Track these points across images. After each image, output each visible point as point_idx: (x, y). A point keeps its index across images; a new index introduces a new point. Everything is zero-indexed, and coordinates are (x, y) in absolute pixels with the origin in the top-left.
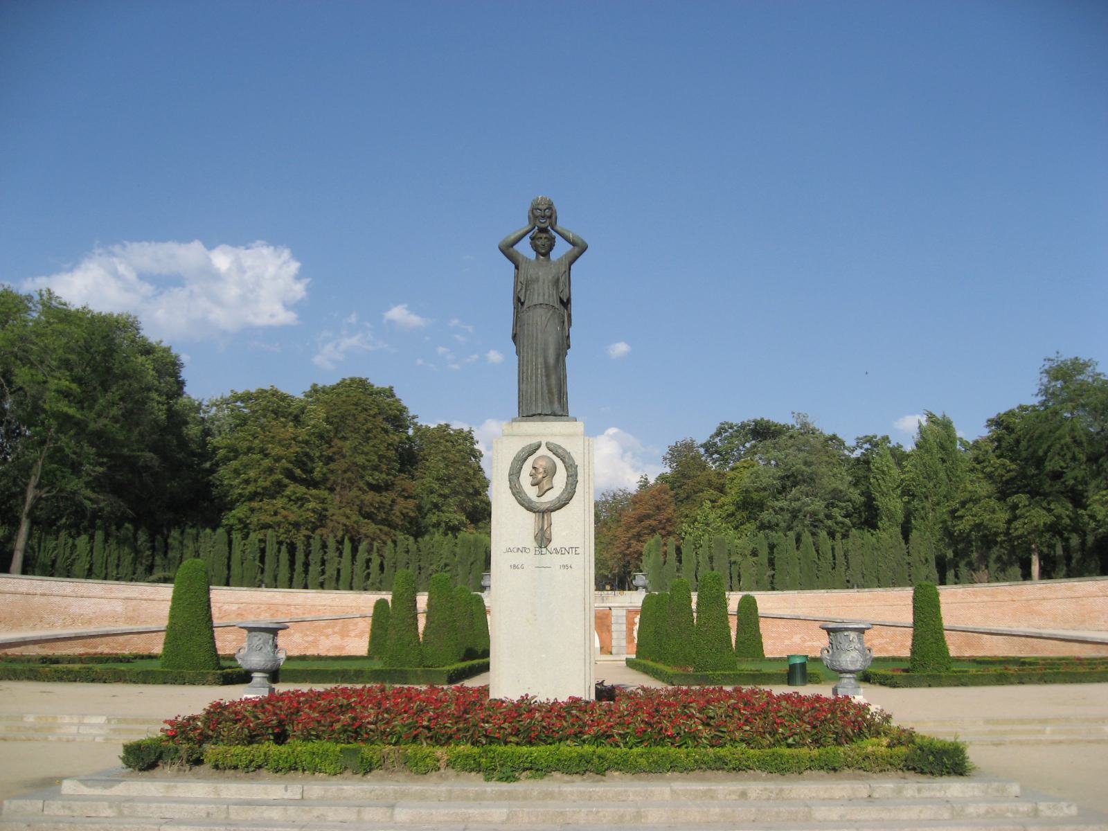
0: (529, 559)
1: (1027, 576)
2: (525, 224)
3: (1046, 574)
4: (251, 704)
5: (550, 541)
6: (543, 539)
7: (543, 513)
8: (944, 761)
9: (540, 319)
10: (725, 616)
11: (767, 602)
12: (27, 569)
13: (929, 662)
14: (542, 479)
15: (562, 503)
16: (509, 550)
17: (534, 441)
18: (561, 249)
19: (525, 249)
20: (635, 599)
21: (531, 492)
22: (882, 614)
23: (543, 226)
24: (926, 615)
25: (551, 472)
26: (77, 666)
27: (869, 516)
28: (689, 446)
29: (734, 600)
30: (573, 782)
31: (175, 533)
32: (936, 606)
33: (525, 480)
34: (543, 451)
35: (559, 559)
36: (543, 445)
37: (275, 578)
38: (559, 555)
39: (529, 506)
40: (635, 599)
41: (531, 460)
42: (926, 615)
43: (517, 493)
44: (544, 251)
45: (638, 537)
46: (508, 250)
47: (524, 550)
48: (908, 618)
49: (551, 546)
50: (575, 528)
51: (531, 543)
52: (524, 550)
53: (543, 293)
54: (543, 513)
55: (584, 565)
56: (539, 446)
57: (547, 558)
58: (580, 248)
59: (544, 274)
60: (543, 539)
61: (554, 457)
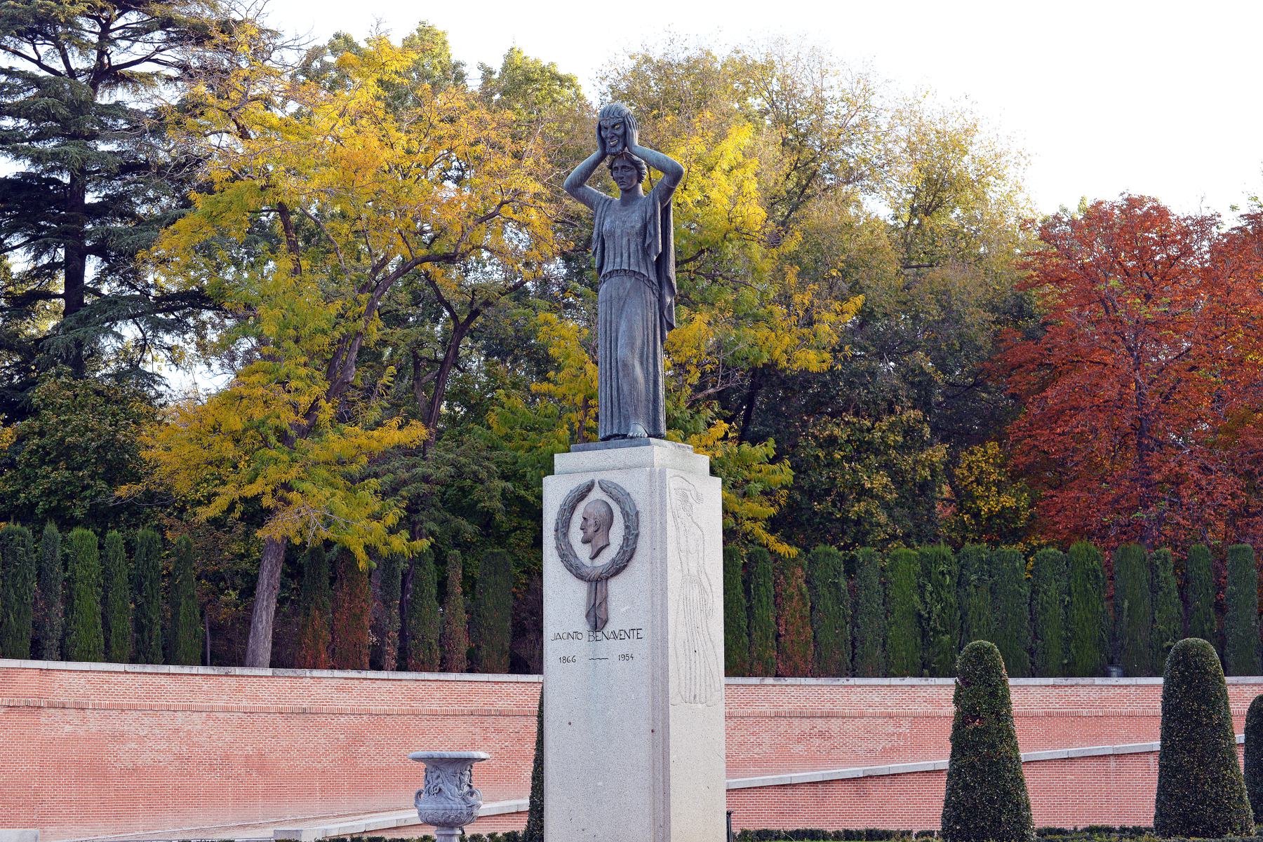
0: (580, 647)
4: (363, 92)
5: (606, 622)
6: (597, 619)
7: (597, 582)
10: (1223, 727)
14: (597, 531)
15: (618, 568)
16: (559, 637)
17: (584, 480)
26: (657, 518)
30: (253, 651)
31: (143, 454)
32: (1005, 700)
33: (576, 535)
34: (596, 494)
36: (597, 485)
38: (618, 641)
39: (576, 570)
41: (581, 507)
43: (566, 555)
47: (575, 635)
49: (609, 628)
51: (582, 626)
52: (575, 635)
54: (597, 582)
56: (590, 488)
57: (612, 648)
60: (597, 619)
61: (610, 501)
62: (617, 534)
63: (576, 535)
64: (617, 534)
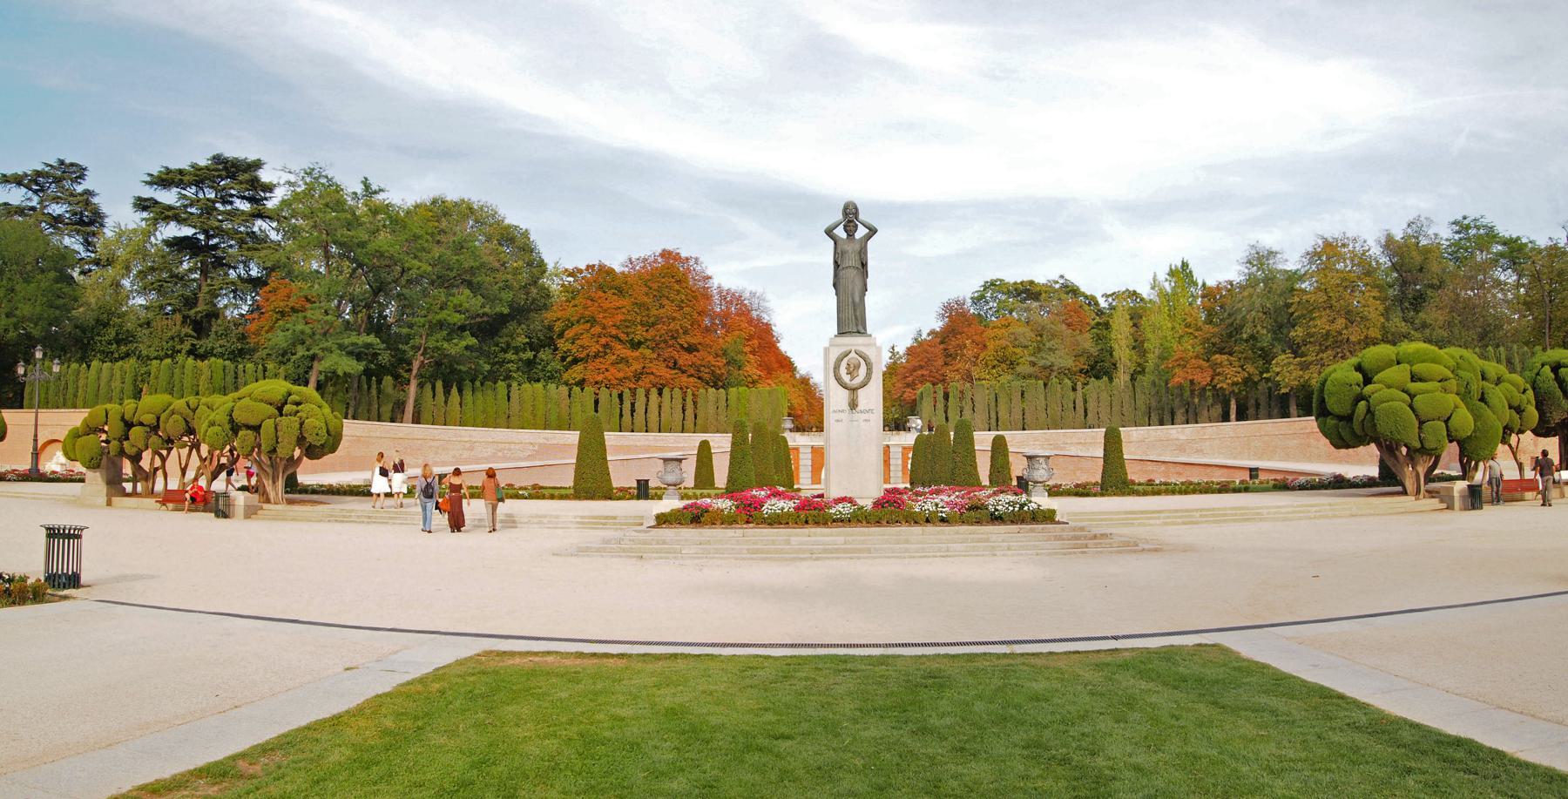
1: (1225, 418)
2: (840, 217)
3: (1241, 416)
6: (853, 405)
8: (66, 598)
9: (851, 275)
11: (1020, 442)
12: (417, 420)
13: (1114, 480)
14: (852, 370)
15: (863, 385)
18: (861, 232)
19: (840, 232)
20: (909, 439)
21: (846, 378)
22: (1087, 444)
23: (851, 215)
24: (1113, 444)
25: (858, 367)
27: (1099, 368)
28: (960, 303)
29: (983, 440)
33: (843, 371)
34: (853, 355)
35: (863, 416)
37: (369, 411)
40: (909, 439)
42: (1113, 444)
44: (850, 234)
45: (912, 385)
46: (829, 232)
48: (1100, 453)
50: (873, 397)
51: (847, 408)
53: (851, 261)
54: (853, 390)
55: (877, 418)
58: (873, 232)
59: (851, 248)
60: (853, 405)
62: (863, 370)
63: (843, 371)
64: (863, 370)
